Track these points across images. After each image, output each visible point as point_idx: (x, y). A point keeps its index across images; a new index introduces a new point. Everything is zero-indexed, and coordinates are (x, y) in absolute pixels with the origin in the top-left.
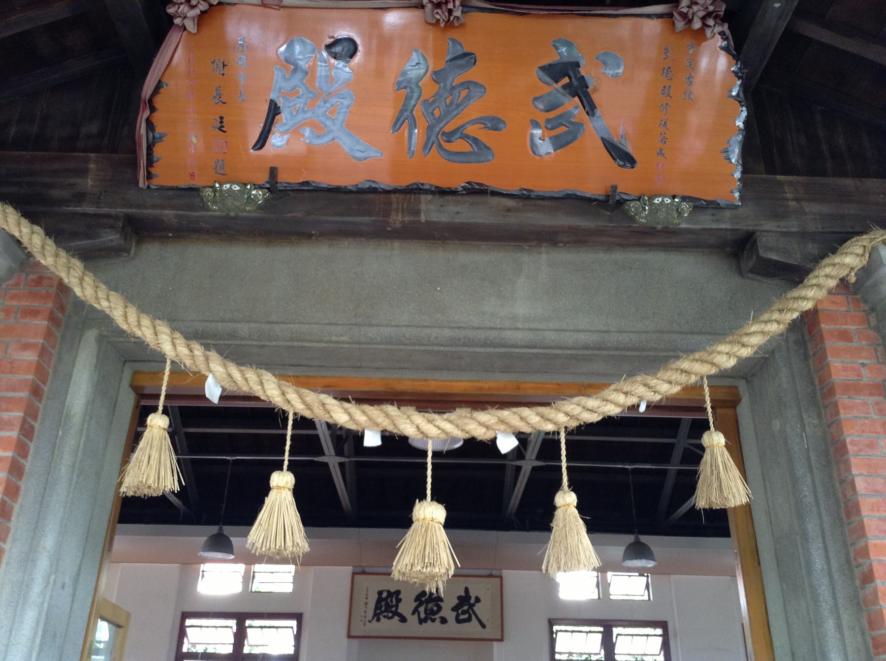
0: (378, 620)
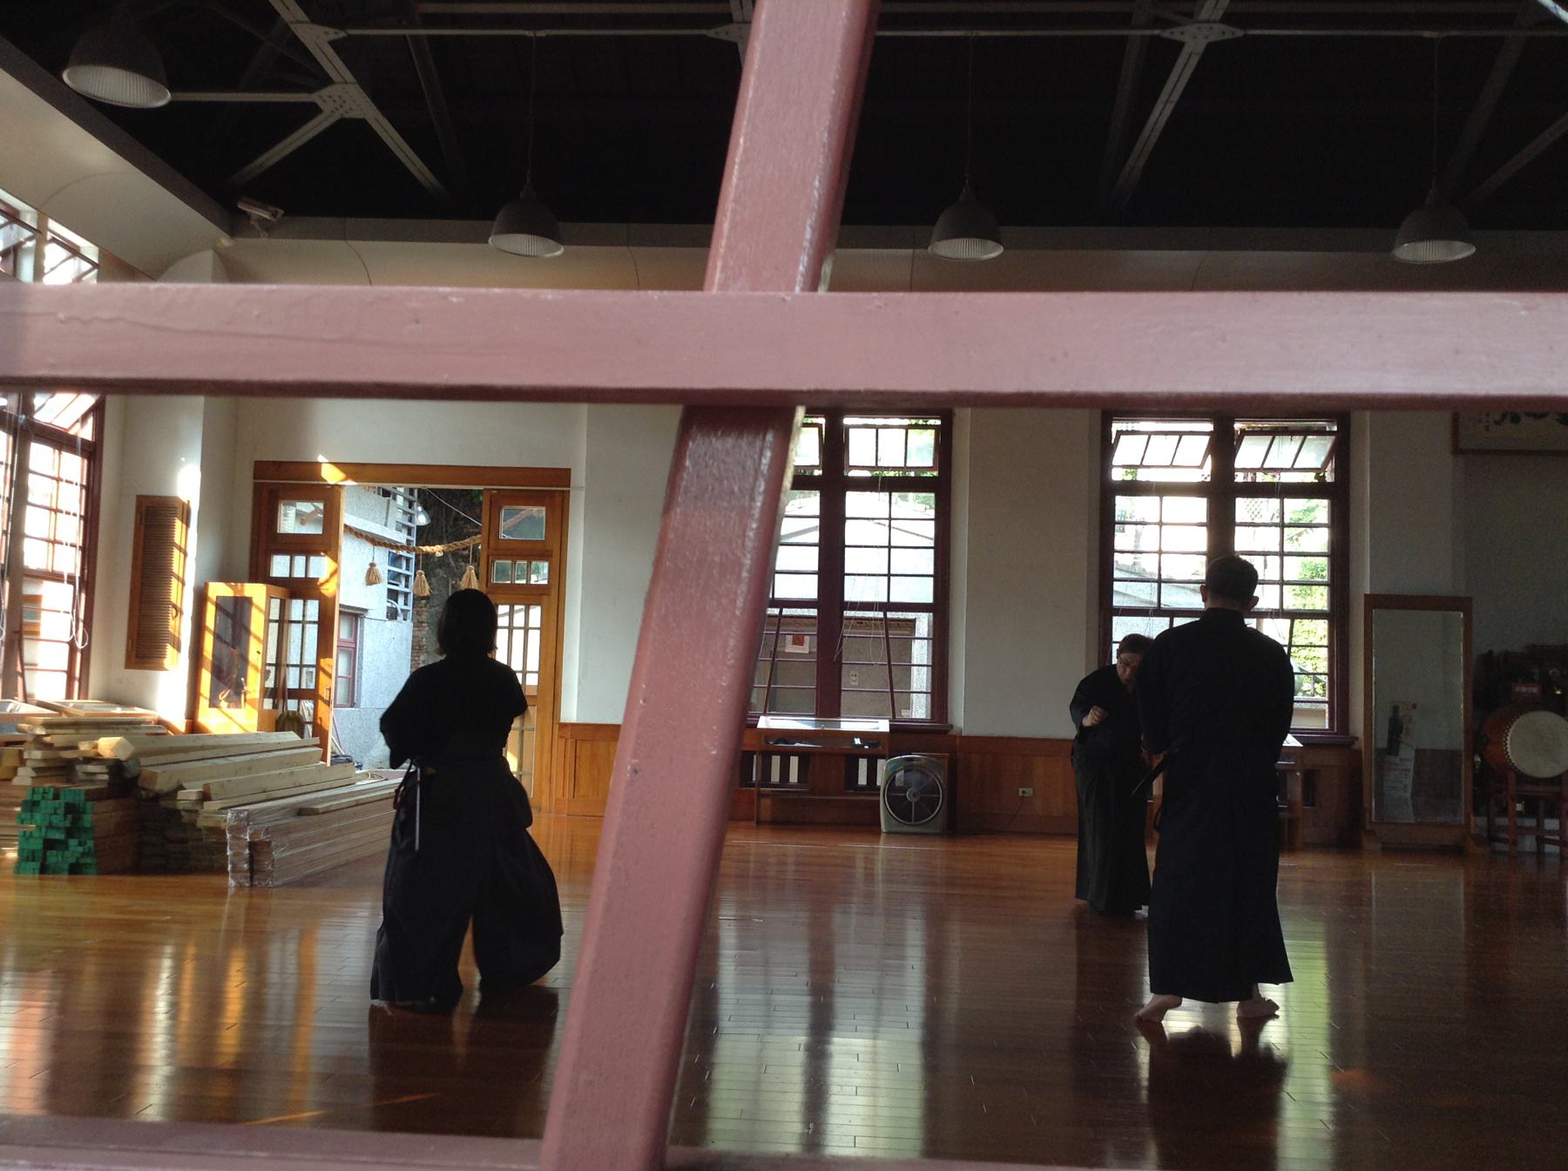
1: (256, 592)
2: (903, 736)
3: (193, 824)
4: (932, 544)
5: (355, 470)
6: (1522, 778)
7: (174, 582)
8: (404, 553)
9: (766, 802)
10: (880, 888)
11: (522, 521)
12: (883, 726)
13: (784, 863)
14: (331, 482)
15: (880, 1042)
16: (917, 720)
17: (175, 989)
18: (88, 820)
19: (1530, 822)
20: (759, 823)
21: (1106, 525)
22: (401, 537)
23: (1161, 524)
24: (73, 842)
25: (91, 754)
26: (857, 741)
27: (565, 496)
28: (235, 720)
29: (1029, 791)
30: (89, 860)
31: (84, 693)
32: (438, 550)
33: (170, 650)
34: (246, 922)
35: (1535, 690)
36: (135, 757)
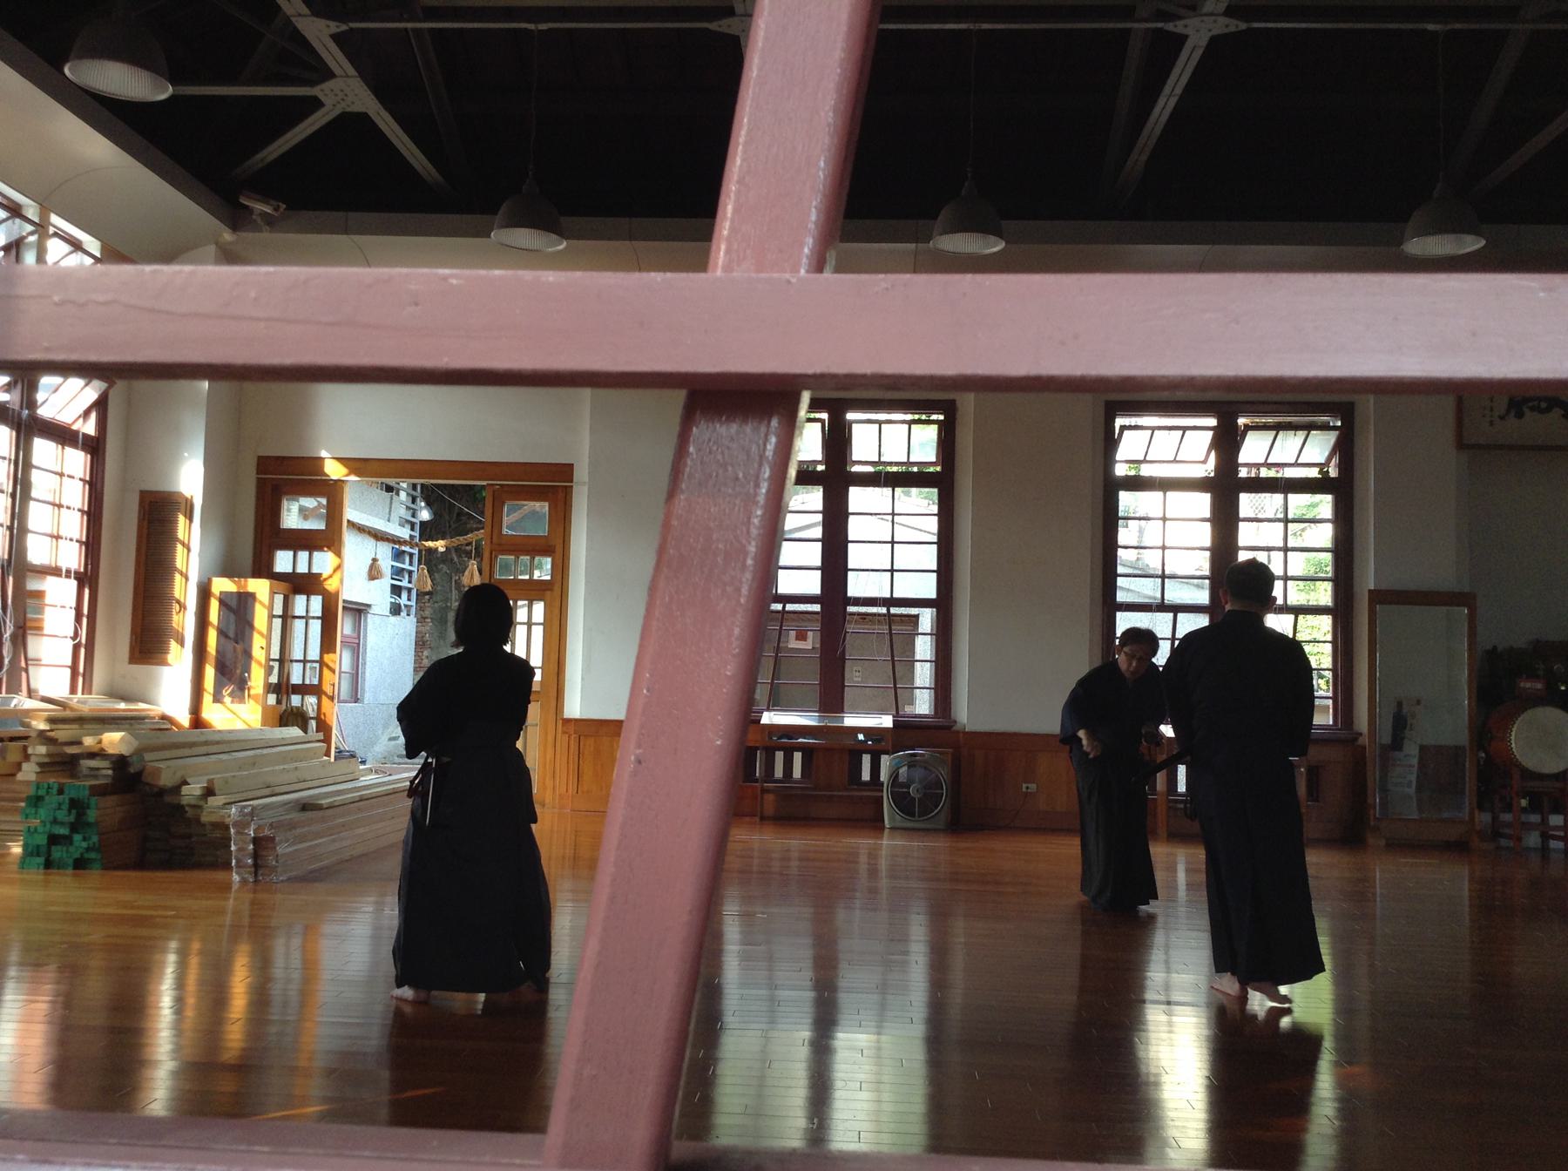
1: (260, 587)
2: (907, 731)
3: (198, 820)
4: (935, 539)
5: (357, 465)
6: (1527, 774)
7: (178, 577)
8: (407, 549)
9: (770, 798)
10: (884, 883)
11: (524, 517)
12: (887, 721)
13: (789, 859)
15: (884, 1038)
16: (920, 716)
17: (180, 984)
18: (92, 815)
19: (1535, 818)
20: (762, 818)
21: (1110, 520)
22: (404, 533)
23: (1164, 519)
24: (77, 838)
25: (95, 750)
26: (861, 737)
27: (568, 491)
28: (236, 716)
29: (1033, 787)
30: (93, 855)
31: (88, 689)
32: (440, 545)
33: (173, 645)
34: (252, 916)
35: (1539, 686)
36: (139, 752)
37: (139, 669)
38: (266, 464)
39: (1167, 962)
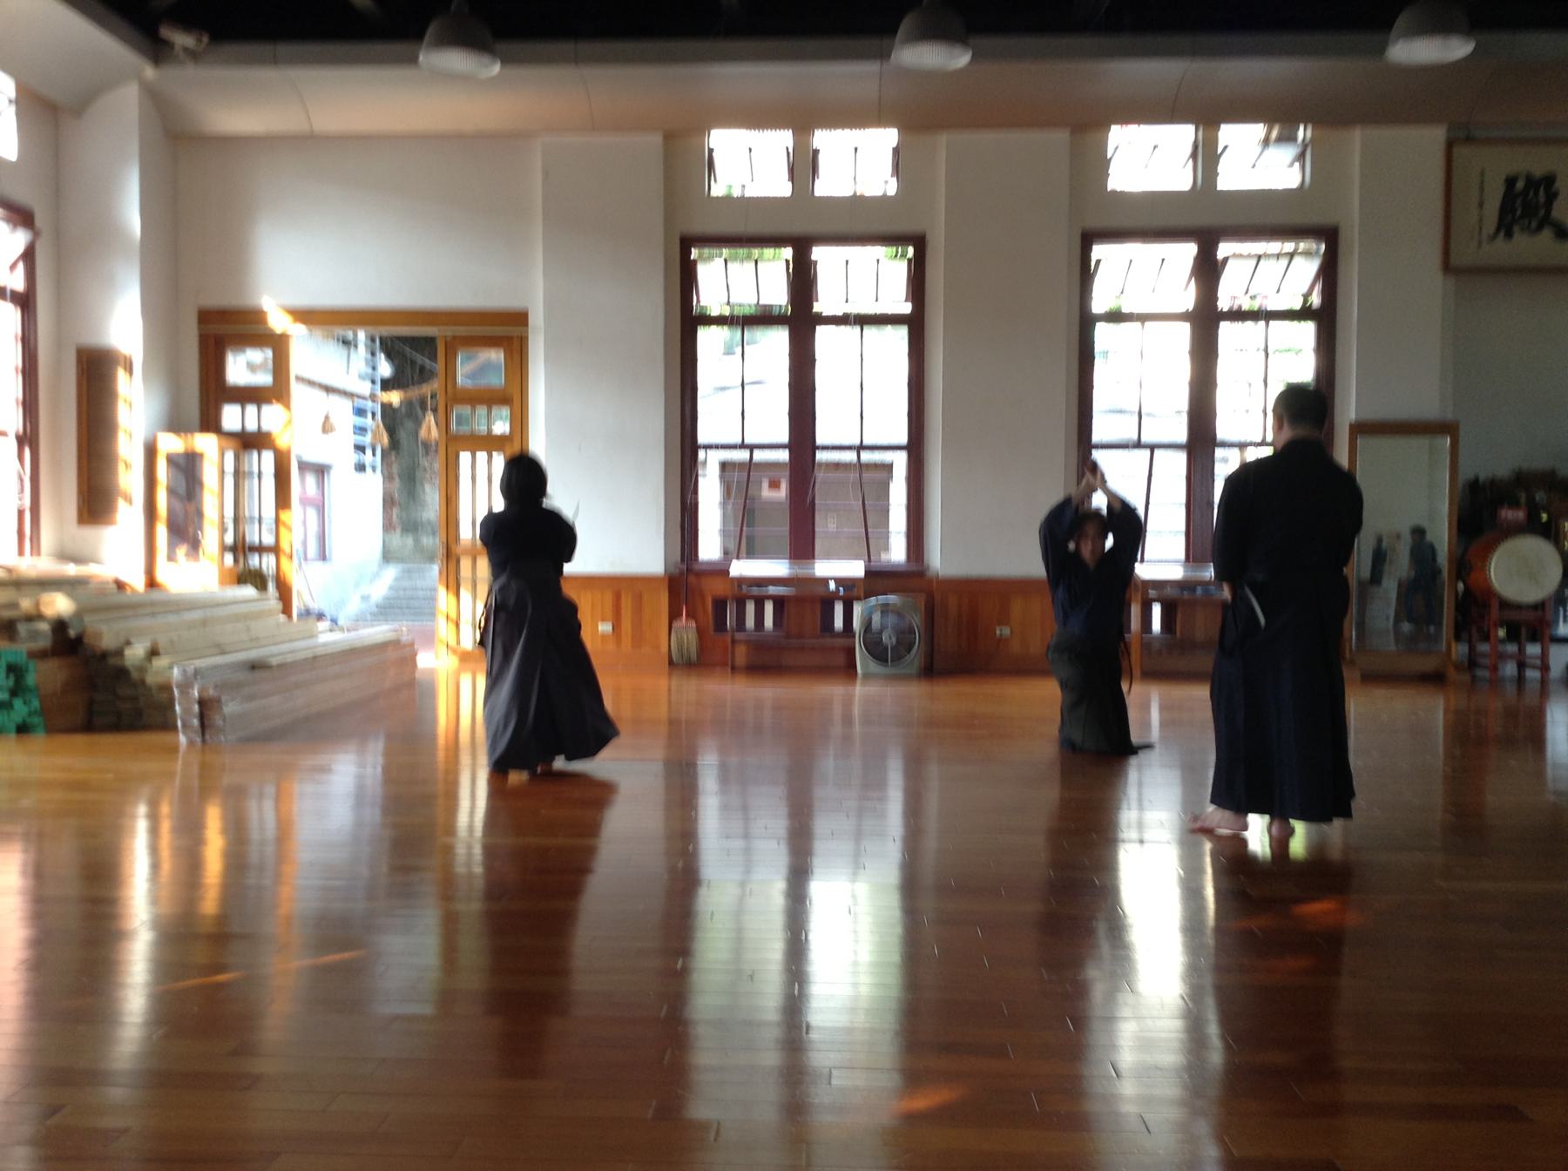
0: (1509, 235)
1: (206, 443)
2: (878, 579)
3: (143, 682)
5: (305, 316)
6: (1505, 604)
11: (476, 367)
14: (278, 331)
18: (31, 680)
19: (1512, 648)
20: (733, 668)
22: (365, 388)
25: (33, 611)
28: (195, 576)
29: (1006, 631)
36: (79, 614)
37: (89, 532)
38: (207, 317)
39: (1140, 800)
